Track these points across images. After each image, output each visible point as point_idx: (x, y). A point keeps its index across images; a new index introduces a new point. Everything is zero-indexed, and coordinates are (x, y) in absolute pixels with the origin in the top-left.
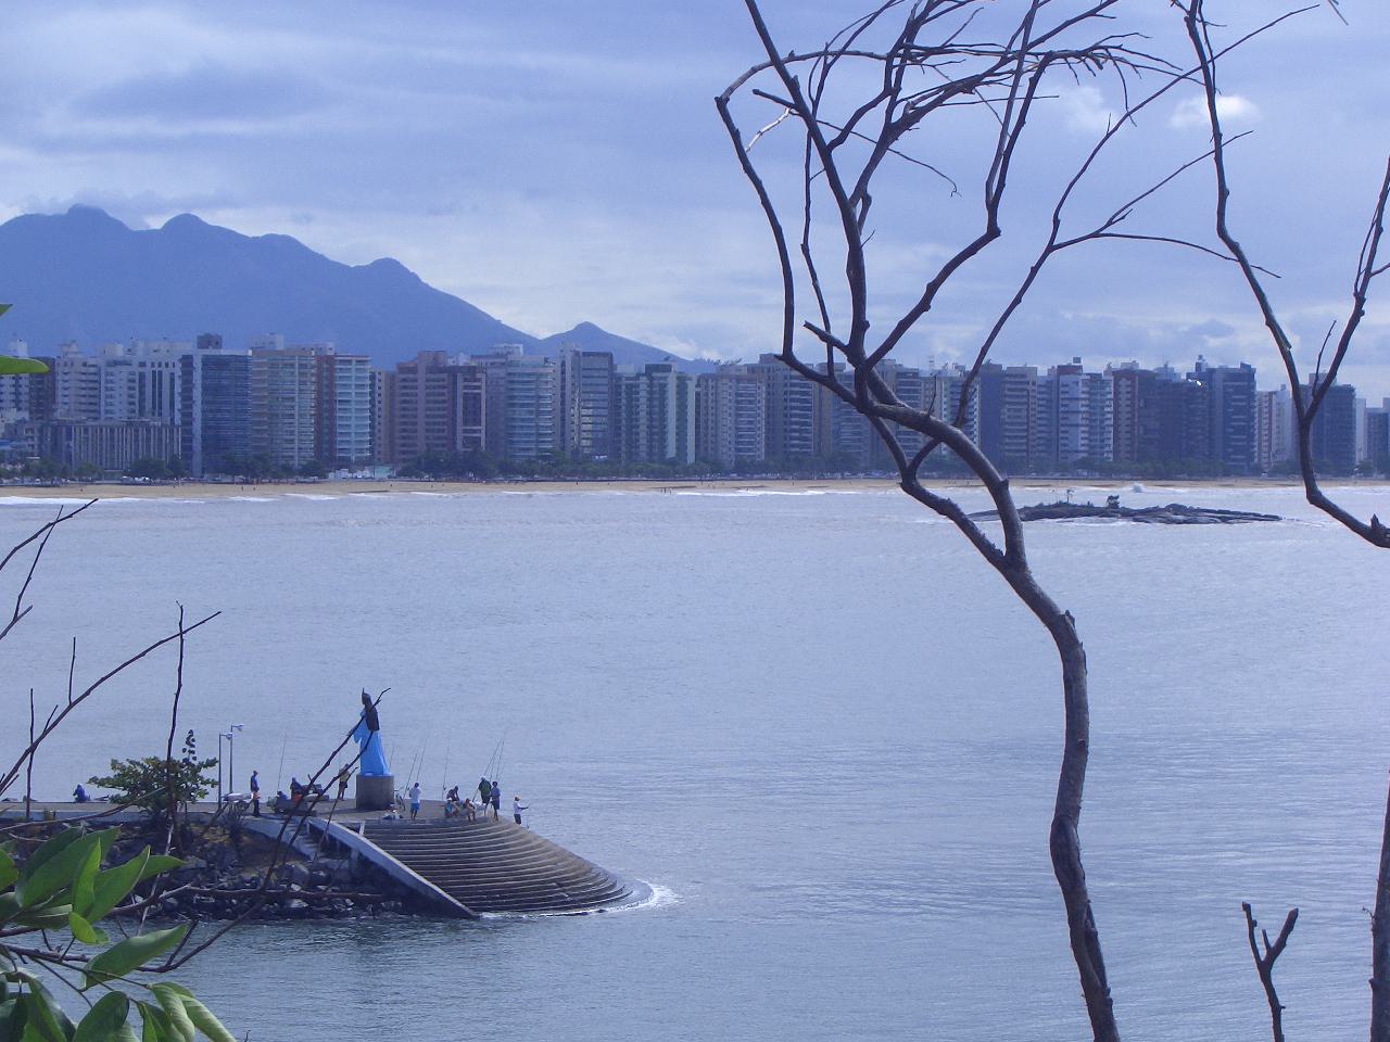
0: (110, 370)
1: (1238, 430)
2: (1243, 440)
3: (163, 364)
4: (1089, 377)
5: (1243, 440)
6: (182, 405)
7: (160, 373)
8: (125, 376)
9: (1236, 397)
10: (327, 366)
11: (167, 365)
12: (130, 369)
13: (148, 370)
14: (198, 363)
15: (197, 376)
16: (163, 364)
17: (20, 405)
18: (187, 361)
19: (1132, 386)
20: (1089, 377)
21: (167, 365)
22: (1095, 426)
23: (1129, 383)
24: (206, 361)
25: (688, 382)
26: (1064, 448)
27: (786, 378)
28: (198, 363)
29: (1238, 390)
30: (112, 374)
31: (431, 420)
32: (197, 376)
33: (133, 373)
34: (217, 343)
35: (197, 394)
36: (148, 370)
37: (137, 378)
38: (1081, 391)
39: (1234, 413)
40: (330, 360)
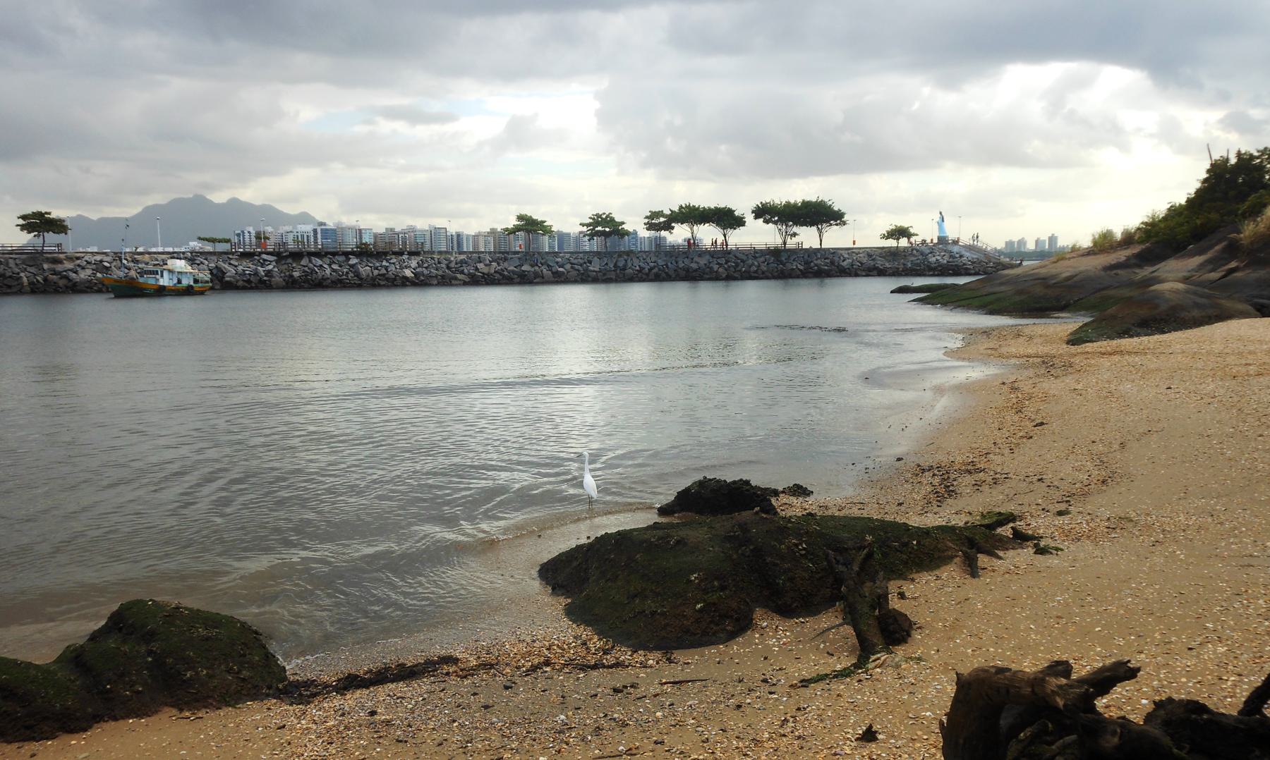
13: (299, 234)
18: (315, 231)
28: (319, 231)
32: (319, 236)
36: (299, 234)
40: (360, 230)
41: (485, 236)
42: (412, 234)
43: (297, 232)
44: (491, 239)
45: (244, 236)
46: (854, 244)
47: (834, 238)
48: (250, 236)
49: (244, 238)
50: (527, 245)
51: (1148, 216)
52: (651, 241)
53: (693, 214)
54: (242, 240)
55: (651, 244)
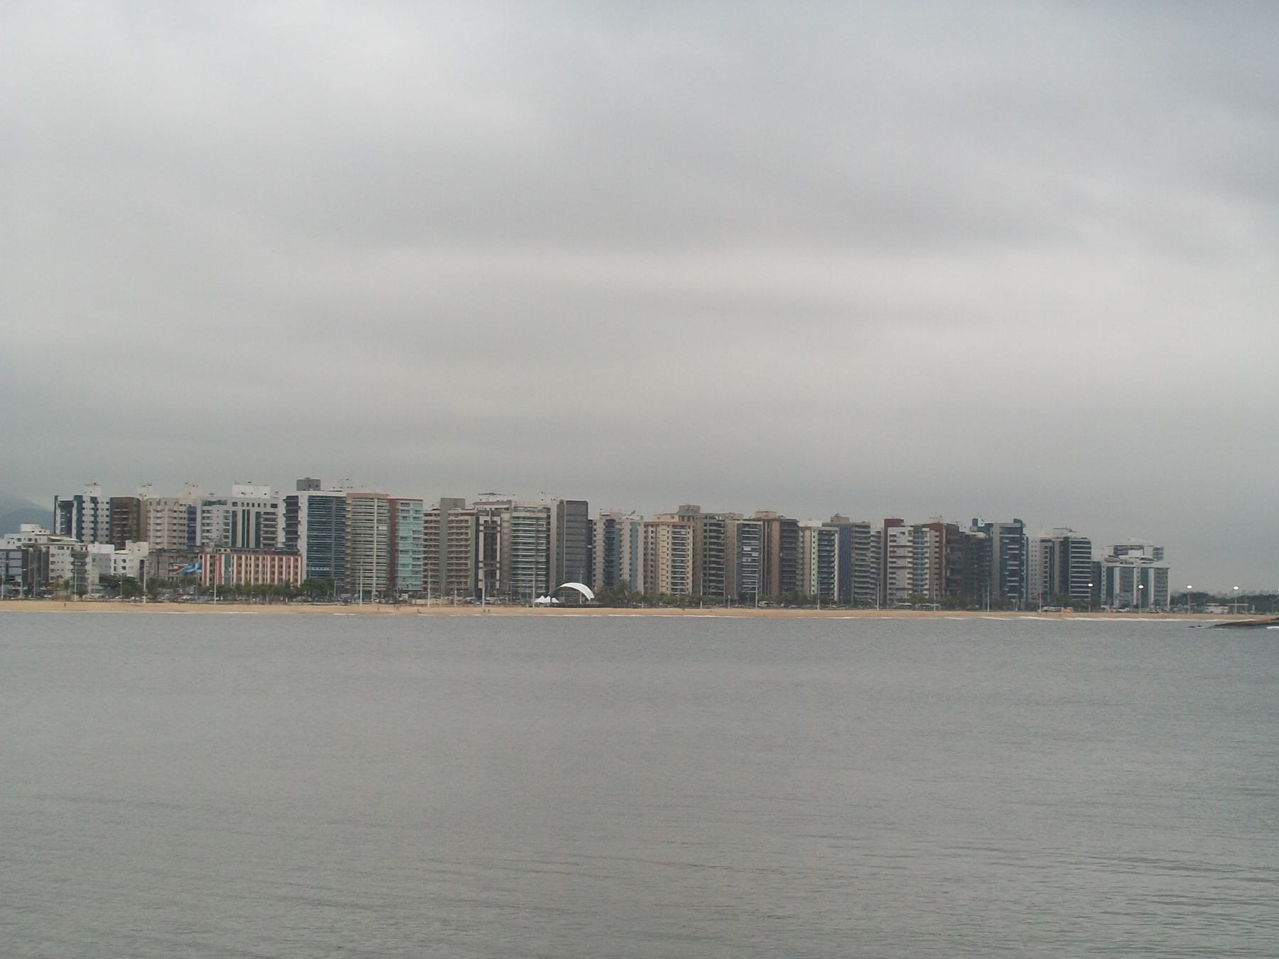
0: (206, 508)
1: (1013, 573)
2: (1016, 549)
3: (251, 505)
4: (912, 529)
5: (1016, 549)
6: (286, 538)
7: (249, 511)
8: (222, 514)
9: (1010, 563)
10: (393, 508)
11: (253, 505)
12: (225, 508)
13: (239, 509)
14: (303, 504)
15: (303, 515)
16: (251, 505)
17: (84, 538)
18: (292, 503)
19: (940, 536)
20: (912, 529)
21: (253, 505)
22: (917, 567)
23: (937, 534)
24: (312, 500)
25: (638, 527)
26: (891, 586)
27: (705, 525)
28: (303, 504)
29: (1013, 541)
30: (208, 512)
31: (793, 535)
32: (303, 515)
33: (227, 512)
34: (317, 486)
35: (303, 530)
36: (239, 509)
37: (231, 514)
38: (904, 540)
39: (1009, 592)
40: (393, 502)
41: (674, 526)
42: (506, 516)
43: (235, 504)
44: (930, 537)
45: (80, 509)
46: (65, 605)
47: (896, 555)
48: (95, 509)
49: (80, 515)
50: (1131, 931)
51: (611, 509)
52: (1052, 549)
53: (33, 542)
54: (74, 518)
55: (1052, 559)
